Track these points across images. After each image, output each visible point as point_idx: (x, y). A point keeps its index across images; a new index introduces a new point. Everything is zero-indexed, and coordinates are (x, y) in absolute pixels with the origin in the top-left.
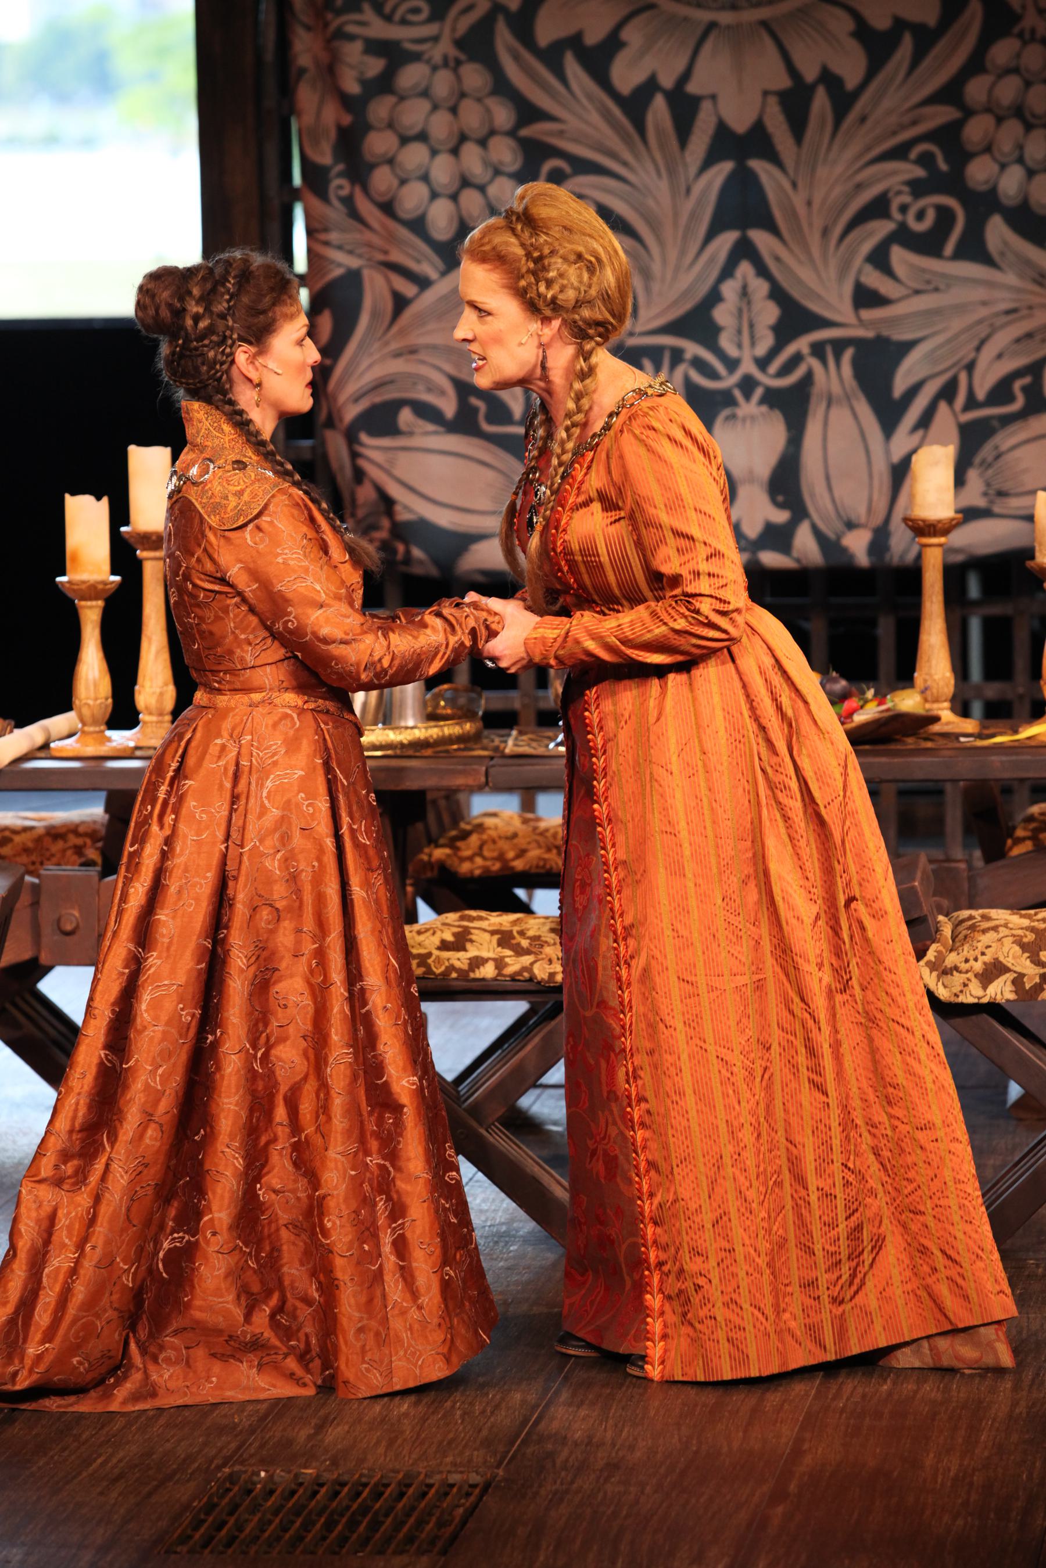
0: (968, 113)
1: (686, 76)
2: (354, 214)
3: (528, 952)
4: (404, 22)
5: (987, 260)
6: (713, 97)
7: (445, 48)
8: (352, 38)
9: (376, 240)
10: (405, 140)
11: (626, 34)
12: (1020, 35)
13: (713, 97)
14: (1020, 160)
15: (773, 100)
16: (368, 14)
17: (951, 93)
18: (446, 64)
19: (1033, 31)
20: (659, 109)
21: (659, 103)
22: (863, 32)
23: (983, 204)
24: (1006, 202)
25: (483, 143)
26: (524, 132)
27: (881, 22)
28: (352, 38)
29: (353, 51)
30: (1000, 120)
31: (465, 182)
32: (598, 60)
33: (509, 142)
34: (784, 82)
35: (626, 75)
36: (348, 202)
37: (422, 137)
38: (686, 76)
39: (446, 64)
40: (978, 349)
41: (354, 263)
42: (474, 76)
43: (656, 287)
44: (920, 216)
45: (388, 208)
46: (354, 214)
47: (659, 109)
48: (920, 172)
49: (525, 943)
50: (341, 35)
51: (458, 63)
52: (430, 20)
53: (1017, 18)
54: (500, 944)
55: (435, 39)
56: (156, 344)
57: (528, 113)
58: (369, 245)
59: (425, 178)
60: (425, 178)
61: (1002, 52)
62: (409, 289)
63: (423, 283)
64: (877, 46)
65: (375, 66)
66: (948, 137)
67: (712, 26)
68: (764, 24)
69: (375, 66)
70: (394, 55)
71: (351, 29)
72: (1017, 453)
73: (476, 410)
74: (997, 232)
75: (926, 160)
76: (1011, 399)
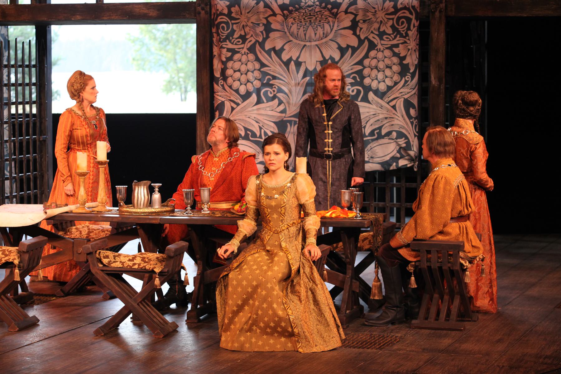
0: (365, 67)
1: (298, 57)
2: (224, 89)
3: (147, 262)
4: (236, 44)
5: (369, 102)
6: (305, 62)
7: (245, 50)
8: (224, 48)
9: (228, 94)
10: (235, 71)
11: (285, 47)
12: (377, 50)
13: (305, 62)
14: (377, 79)
15: (318, 63)
16: (228, 42)
17: (360, 63)
18: (245, 54)
19: (380, 49)
20: (292, 65)
21: (292, 63)
22: (340, 48)
23: (368, 89)
24: (373, 88)
25: (253, 72)
26: (262, 70)
27: (344, 46)
28: (224, 48)
29: (224, 51)
30: (372, 69)
31: (248, 81)
32: (279, 53)
33: (259, 72)
34: (322, 59)
35: (285, 57)
36: (223, 86)
37: (239, 71)
38: (298, 57)
39: (245, 54)
40: (366, 123)
41: (223, 100)
42: (251, 57)
43: (291, 106)
44: (353, 91)
45: (230, 87)
46: (224, 89)
47: (292, 65)
48: (353, 81)
49: (147, 260)
50: (222, 47)
51: (248, 53)
52: (242, 44)
53: (376, 46)
54: (142, 260)
55: (243, 48)
56: (396, 182)
57: (263, 65)
58: (227, 96)
59: (239, 80)
60: (239, 80)
61: (373, 53)
62: (235, 106)
63: (238, 104)
64: (343, 51)
65: (229, 54)
66: (360, 73)
67: (305, 45)
68: (316, 45)
69: (229, 54)
70: (234, 52)
71: (224, 46)
72: (375, 148)
73: (249, 134)
74: (371, 95)
75: (354, 78)
76: (374, 135)
